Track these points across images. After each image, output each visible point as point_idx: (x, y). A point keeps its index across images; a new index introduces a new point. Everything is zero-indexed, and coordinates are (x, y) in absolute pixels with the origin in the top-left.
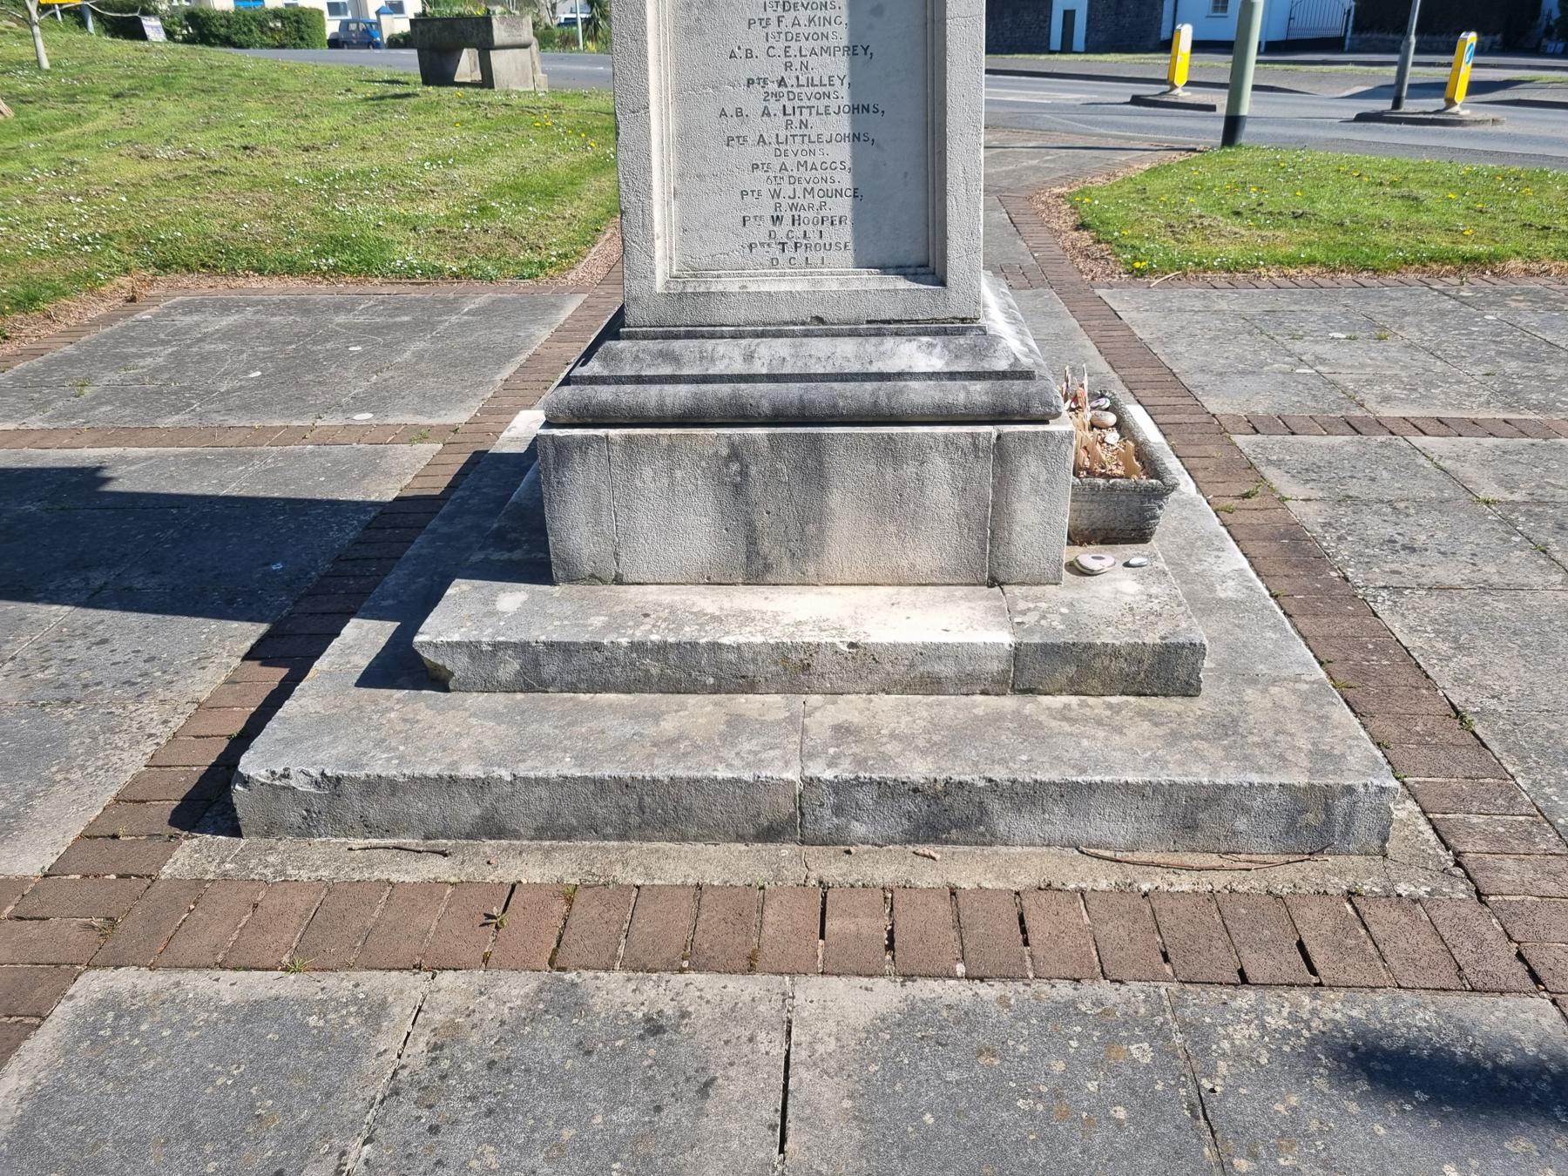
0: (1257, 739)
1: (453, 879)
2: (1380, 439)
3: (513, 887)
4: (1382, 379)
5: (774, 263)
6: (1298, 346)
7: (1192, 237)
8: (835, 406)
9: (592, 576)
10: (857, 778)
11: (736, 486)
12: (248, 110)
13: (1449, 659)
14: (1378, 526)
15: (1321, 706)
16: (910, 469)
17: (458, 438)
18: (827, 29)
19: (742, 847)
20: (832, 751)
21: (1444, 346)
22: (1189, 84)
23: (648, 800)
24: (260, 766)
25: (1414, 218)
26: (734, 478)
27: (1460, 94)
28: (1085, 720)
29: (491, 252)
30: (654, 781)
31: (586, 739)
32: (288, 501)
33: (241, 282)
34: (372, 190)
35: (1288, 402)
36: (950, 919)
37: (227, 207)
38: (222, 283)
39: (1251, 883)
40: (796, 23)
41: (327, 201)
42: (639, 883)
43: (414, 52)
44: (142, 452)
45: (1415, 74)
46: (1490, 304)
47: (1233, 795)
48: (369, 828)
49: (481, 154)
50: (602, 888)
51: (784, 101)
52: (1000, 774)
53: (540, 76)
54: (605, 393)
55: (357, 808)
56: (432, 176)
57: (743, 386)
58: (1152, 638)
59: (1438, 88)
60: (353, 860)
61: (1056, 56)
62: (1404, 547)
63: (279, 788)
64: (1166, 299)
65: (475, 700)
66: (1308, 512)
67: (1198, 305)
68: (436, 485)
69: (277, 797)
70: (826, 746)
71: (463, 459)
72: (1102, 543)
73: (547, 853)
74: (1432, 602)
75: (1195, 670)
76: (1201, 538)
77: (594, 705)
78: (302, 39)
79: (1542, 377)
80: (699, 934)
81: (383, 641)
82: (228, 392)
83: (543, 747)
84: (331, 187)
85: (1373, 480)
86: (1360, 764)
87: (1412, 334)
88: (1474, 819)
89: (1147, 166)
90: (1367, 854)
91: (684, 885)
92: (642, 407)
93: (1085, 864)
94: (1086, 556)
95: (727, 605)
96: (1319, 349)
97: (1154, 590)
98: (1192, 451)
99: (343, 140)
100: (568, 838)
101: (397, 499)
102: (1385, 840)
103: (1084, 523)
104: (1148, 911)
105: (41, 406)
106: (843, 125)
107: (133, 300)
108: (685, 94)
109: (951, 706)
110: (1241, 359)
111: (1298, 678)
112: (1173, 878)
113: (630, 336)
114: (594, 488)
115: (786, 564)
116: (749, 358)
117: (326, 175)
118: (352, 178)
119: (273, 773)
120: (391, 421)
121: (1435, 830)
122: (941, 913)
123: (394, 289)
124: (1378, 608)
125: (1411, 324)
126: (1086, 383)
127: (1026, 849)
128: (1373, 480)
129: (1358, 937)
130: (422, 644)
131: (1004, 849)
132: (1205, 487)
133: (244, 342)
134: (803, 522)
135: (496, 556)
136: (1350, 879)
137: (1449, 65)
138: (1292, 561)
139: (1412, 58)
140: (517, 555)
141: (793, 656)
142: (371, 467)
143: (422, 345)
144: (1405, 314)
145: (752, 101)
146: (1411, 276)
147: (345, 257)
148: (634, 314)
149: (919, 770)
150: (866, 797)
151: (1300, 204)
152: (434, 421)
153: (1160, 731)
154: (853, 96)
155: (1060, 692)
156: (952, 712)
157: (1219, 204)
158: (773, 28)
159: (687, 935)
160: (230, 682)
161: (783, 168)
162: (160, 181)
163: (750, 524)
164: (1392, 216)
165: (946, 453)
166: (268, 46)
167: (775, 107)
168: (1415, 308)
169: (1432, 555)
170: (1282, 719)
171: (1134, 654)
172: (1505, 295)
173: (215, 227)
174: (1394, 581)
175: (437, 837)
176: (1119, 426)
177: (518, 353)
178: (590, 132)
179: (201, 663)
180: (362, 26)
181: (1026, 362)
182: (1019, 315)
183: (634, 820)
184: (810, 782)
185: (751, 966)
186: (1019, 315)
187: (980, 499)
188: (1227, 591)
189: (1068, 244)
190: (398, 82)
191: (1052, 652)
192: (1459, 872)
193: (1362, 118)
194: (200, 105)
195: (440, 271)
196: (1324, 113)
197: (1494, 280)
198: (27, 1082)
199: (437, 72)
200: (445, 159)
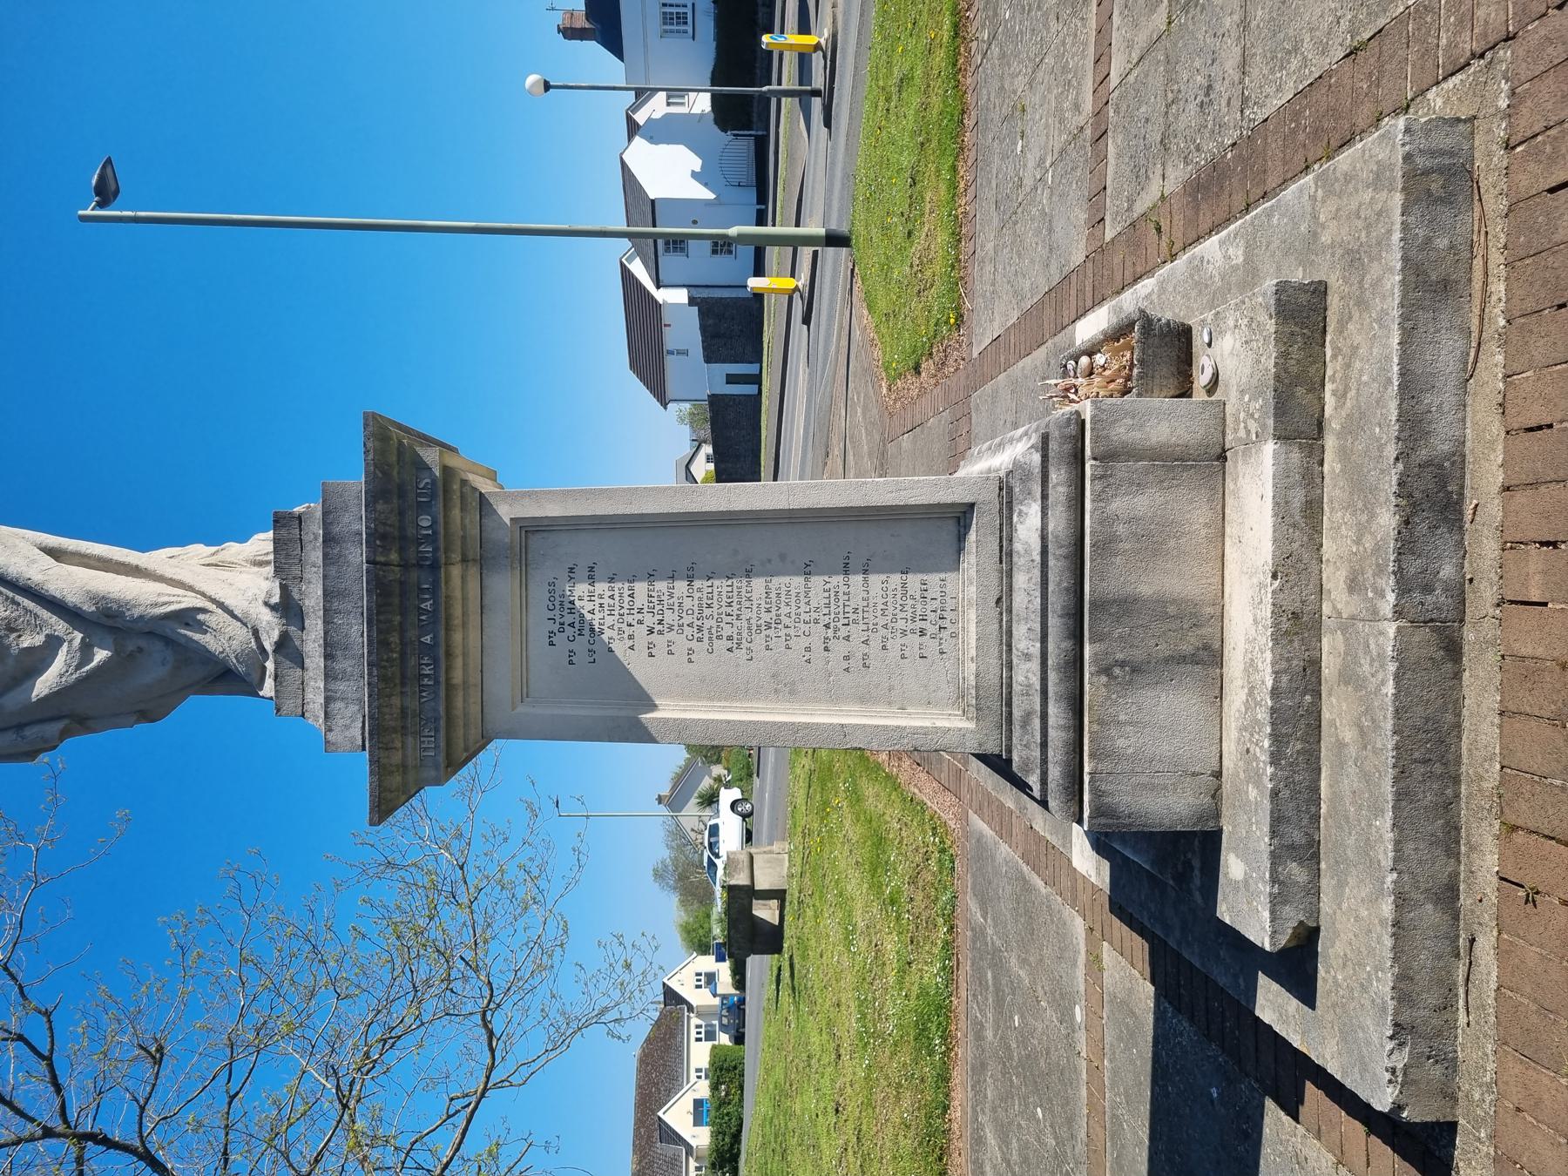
0: (1363, 234)
1: (1495, 933)
2: (1111, 114)
3: (1502, 879)
4: (1059, 110)
5: (954, 636)
6: (1028, 182)
7: (928, 273)
8: (1067, 589)
9: (1213, 797)
10: (1394, 573)
11: (1133, 671)
12: (803, 1110)
13: (1305, 58)
14: (1189, 116)
15: (1337, 180)
16: (1121, 529)
17: (1098, 927)
18: (793, 593)
19: (1466, 674)
20: (1370, 595)
21: (1032, 55)
22: (793, 275)
23: (1416, 755)
24: (1384, 1092)
25: (917, 81)
26: (1130, 672)
27: (810, 40)
28: (1346, 378)
29: (931, 895)
30: (1397, 748)
31: (1360, 808)
33: (955, 1126)
34: (875, 999)
35: (1077, 192)
36: (1529, 492)
37: (890, 1131)
38: (957, 1144)
39: (1498, 231)
40: (789, 615)
41: (884, 1041)
42: (1498, 767)
43: (749, 960)
45: (789, 81)
46: (996, 14)
47: (1413, 253)
48: (1447, 1006)
49: (844, 901)
50: (1502, 800)
51: (839, 625)
52: (1391, 451)
53: (776, 847)
54: (1055, 772)
55: (1426, 1013)
56: (863, 945)
57: (1050, 662)
58: (1271, 326)
59: (804, 60)
60: (1478, 1023)
61: (764, 390)
62: (1207, 94)
63: (1406, 1079)
64: (984, 296)
65: (1326, 905)
66: (1172, 178)
67: (989, 268)
68: (1139, 946)
69: (1414, 1082)
70: (1366, 599)
71: (1117, 922)
72: (1190, 365)
73: (1472, 848)
74: (1255, 72)
75: (1302, 288)
76: (1192, 276)
77: (1331, 800)
78: (735, 1068)
80: (1543, 713)
81: (1275, 986)
82: (1056, 1138)
83: (1367, 846)
84: (872, 1035)
85: (1147, 120)
86: (1385, 146)
87: (1020, 83)
88: (1444, 41)
89: (866, 312)
90: (1472, 133)
91: (1500, 726)
92: (1066, 743)
93: (1482, 373)
94: (1202, 379)
95: (1239, 682)
96: (1031, 164)
97: (1231, 323)
98: (1118, 277)
99: (830, 1024)
100: (1458, 829)
101: (1153, 982)
102: (1458, 120)
103: (1173, 383)
104: (1523, 320)
106: (856, 579)
108: (834, 697)
109: (1333, 491)
110: (1038, 232)
111: (1313, 198)
112: (1494, 298)
113: (1009, 751)
114: (1134, 787)
115: (1203, 631)
116: (1027, 657)
117: (861, 1040)
118: (864, 1016)
119: (1390, 1081)
120: (1082, 989)
121: (1452, 74)
122: (1524, 500)
123: (963, 985)
124: (1260, 117)
125: (1012, 83)
126: (1053, 382)
127: (1468, 424)
128: (1147, 120)
129: (1544, 143)
130: (1272, 944)
131: (1468, 444)
132: (1150, 265)
133: (1010, 1123)
134: (1167, 617)
135: (1197, 882)
136: (1495, 147)
138: (1219, 192)
139: (774, 87)
140: (1196, 863)
141: (1285, 626)
142: (1124, 1006)
143: (1013, 961)
144: (1002, 88)
145: (840, 648)
146: (969, 81)
147: (934, 1029)
148: (991, 747)
149: (1387, 520)
150: (1413, 566)
152: (1083, 949)
153: (1356, 315)
154: (837, 573)
155: (1321, 399)
156: (1338, 492)
157: (900, 250)
158: (792, 632)
159: (1544, 723)
160: (1318, 1136)
161: (885, 626)
163: (1167, 660)
164: (916, 101)
165: (1108, 501)
166: (741, 1100)
167: (843, 632)
168: (999, 79)
169: (1215, 70)
170: (1346, 211)
173: (907, 1144)
174: (1236, 103)
175: (1457, 946)
176: (1090, 354)
177: (1021, 872)
178: (826, 803)
179: (1301, 1161)
180: (724, 1012)
181: (1035, 439)
182: (997, 440)
183: (1438, 768)
184: (1399, 613)
186: (997, 440)
187: (1147, 472)
188: (1238, 255)
189: (933, 381)
190: (779, 975)
191: (1283, 406)
192: (1489, 55)
195: (946, 943)
196: (822, 154)
197: (974, 9)
200: (848, 933)
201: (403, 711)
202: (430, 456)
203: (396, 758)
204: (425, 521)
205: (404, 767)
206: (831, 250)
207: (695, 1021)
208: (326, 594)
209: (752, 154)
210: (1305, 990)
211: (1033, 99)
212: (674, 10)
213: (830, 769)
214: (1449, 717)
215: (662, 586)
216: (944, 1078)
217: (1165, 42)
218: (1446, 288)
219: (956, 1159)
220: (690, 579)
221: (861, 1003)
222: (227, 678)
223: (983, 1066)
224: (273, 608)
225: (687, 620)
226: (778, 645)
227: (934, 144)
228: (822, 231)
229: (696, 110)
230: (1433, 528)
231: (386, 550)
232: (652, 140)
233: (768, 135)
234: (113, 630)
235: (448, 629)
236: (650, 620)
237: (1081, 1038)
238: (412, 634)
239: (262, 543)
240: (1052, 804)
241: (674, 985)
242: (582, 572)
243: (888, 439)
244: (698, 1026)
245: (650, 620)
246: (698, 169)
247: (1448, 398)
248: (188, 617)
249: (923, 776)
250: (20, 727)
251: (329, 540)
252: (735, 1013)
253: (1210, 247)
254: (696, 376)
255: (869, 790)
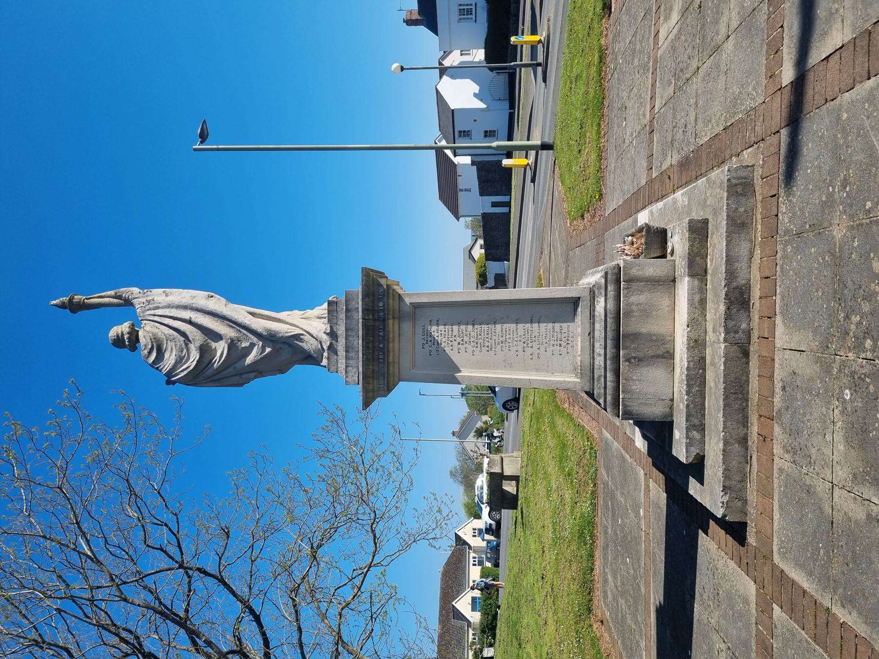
5: (572, 347)
6: (627, 142)
14: (679, 136)
16: (634, 308)
22: (526, 157)
26: (638, 361)
27: (536, 38)
30: (724, 388)
32: (666, 534)
35: (644, 153)
44: (652, 596)
45: (526, 60)
52: (723, 283)
53: (514, 454)
54: (609, 398)
56: (555, 496)
59: (534, 48)
61: (513, 210)
63: (727, 505)
66: (673, 159)
67: (612, 176)
68: (661, 477)
75: (699, 221)
79: (640, 52)
86: (720, 174)
87: (625, 94)
92: (613, 387)
99: (540, 537)
100: (747, 418)
105: (637, 642)
107: (602, 622)
108: (526, 369)
113: (593, 390)
116: (600, 355)
118: (555, 530)
123: (600, 510)
134: (652, 340)
137: (522, 46)
142: (657, 505)
145: (529, 351)
148: (587, 389)
149: (722, 308)
150: (731, 324)
151: (576, 125)
155: (706, 262)
162: (555, 613)
163: (652, 357)
165: (629, 297)
166: (497, 596)
167: (530, 345)
171: (691, 240)
172: (613, 51)
173: (574, 587)
174: (694, 135)
175: (746, 459)
178: (539, 429)
183: (740, 396)
184: (725, 340)
185: (773, 360)
191: (691, 264)
193: (545, 80)
194: (525, 607)
195: (593, 492)
198: (793, 570)
199: (511, 502)
200: (548, 491)
201: (373, 370)
202: (383, 281)
203: (371, 387)
204: (381, 304)
205: (373, 390)
206: (545, 152)
207: (472, 555)
208: (347, 330)
209: (507, 83)
210: (701, 480)
211: (629, 104)
212: (465, 7)
213: (541, 412)
214: (744, 378)
215: (463, 327)
216: (591, 556)
217: (672, 101)
218: (743, 225)
219: (597, 593)
220: (473, 325)
221: (554, 524)
222: (311, 359)
223: (607, 545)
224: (327, 334)
225: (472, 340)
226: (506, 349)
227: (591, 111)
228: (539, 143)
229: (477, 59)
230: (738, 311)
231: (368, 315)
232: (453, 77)
233: (515, 72)
234: (272, 341)
235: (388, 342)
236: (459, 340)
237: (643, 522)
238: (377, 344)
239: (322, 309)
240: (608, 410)
241: (460, 534)
242: (434, 322)
243: (570, 249)
244: (474, 558)
245: (459, 340)
246: (477, 92)
247: (744, 265)
248: (297, 337)
249: (584, 413)
250: (241, 374)
251: (347, 310)
252: (495, 551)
253: (679, 194)
254: (474, 202)
255: (559, 421)
